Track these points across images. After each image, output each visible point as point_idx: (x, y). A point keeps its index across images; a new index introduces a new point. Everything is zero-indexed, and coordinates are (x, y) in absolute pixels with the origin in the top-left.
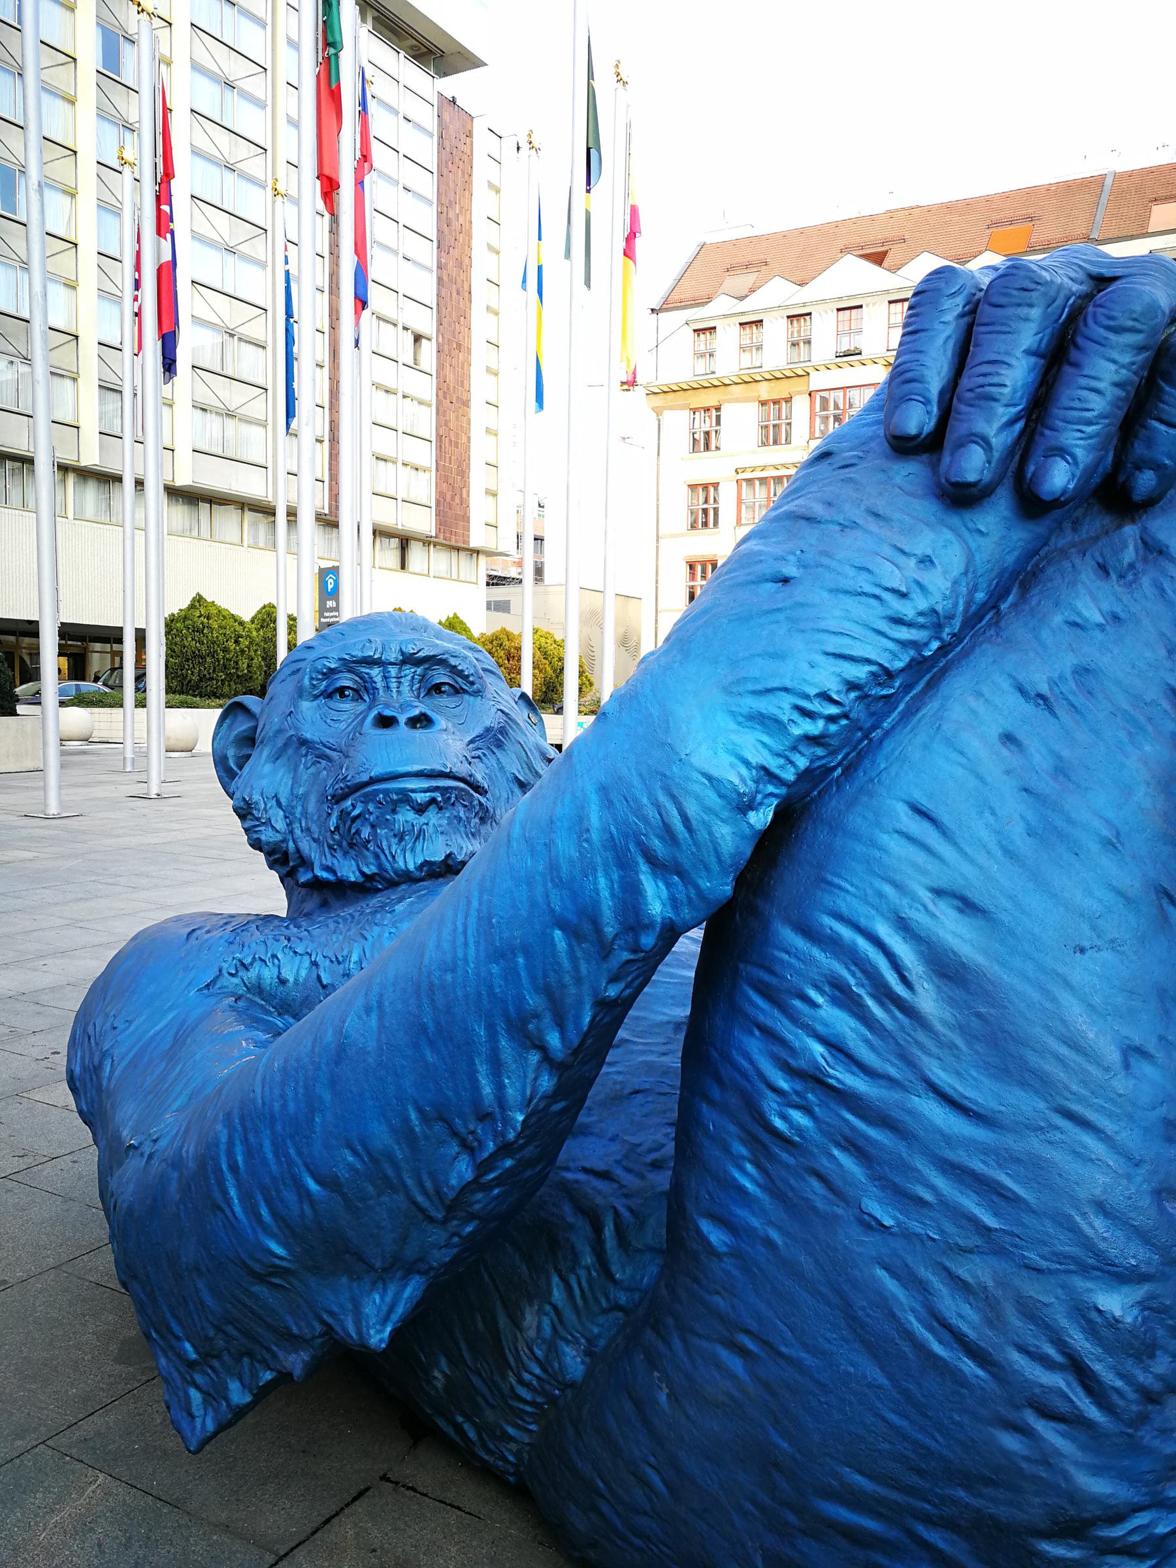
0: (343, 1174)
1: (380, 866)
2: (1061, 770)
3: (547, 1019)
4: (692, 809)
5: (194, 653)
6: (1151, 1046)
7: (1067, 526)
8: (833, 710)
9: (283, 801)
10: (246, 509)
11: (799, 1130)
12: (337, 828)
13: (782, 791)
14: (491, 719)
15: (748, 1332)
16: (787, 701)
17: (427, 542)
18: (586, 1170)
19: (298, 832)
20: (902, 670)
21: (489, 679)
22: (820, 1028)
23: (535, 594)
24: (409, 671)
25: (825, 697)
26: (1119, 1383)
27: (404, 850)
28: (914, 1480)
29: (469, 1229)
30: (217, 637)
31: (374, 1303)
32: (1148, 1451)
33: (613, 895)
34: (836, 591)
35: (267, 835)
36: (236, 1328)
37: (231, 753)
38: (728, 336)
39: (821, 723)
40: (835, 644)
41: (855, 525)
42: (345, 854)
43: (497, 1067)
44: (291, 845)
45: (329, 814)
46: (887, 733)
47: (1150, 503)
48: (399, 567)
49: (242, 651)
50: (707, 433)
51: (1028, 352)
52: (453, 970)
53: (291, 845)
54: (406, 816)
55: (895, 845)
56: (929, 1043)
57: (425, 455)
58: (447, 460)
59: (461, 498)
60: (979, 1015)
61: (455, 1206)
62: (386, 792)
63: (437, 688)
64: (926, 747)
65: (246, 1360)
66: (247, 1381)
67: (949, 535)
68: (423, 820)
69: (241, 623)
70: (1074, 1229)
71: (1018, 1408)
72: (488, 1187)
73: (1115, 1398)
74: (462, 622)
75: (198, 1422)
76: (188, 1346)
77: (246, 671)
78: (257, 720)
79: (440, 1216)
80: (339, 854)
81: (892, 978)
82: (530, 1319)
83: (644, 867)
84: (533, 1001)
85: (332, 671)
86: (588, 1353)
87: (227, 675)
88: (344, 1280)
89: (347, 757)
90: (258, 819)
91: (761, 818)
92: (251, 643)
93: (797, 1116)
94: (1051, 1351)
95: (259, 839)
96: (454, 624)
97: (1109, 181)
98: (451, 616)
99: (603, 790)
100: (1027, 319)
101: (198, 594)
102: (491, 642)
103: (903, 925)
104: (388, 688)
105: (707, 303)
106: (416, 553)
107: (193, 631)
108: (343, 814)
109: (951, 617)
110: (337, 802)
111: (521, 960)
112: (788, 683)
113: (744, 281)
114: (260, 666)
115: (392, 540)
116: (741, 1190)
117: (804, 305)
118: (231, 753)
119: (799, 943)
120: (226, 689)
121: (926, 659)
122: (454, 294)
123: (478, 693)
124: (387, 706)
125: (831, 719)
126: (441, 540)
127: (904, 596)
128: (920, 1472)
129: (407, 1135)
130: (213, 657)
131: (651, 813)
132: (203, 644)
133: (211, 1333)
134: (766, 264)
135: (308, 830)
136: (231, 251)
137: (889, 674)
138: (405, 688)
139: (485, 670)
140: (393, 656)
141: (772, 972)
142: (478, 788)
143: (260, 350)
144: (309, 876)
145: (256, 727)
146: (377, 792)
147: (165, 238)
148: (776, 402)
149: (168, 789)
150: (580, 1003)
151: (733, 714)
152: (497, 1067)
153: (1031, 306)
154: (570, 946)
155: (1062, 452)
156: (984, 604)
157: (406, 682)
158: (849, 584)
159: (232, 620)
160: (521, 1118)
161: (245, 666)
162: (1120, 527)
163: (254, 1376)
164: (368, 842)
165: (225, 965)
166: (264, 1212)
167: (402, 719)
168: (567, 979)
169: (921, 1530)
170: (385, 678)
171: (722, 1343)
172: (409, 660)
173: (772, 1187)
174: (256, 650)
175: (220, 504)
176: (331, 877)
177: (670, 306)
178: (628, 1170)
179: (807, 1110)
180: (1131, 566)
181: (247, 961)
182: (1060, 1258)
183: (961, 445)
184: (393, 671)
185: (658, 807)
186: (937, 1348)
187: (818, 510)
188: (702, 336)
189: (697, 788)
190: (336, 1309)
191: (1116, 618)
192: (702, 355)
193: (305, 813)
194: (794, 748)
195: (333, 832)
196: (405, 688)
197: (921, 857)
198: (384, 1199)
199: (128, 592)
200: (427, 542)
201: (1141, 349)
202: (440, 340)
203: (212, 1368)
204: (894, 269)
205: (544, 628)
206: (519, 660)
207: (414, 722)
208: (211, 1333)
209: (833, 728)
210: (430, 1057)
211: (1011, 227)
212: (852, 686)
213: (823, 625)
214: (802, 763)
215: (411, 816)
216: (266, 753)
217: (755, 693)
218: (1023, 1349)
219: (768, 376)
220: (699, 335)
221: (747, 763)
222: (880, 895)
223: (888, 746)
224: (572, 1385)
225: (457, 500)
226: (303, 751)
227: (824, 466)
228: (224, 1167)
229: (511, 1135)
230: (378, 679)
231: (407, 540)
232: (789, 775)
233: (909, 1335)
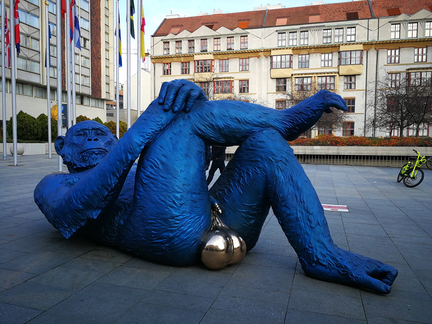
0: (90, 195)
1: (90, 164)
2: (176, 142)
3: (117, 172)
4: (134, 146)
5: (20, 127)
6: (183, 170)
7: (180, 114)
8: (151, 135)
9: (71, 154)
10: (34, 86)
11: (147, 182)
12: (81, 158)
13: (145, 144)
14: (109, 140)
15: (141, 206)
16: (145, 134)
17: (89, 97)
18: (124, 199)
19: (73, 159)
20: (159, 130)
21: (108, 132)
22: (149, 171)
23: (120, 111)
24: (93, 131)
25: (149, 133)
26: (178, 203)
27: (94, 161)
28: (157, 216)
29: (107, 203)
30: (27, 123)
31: (94, 213)
32: (181, 210)
33: (125, 157)
34: (151, 121)
35: (68, 160)
36: (74, 220)
37: (58, 146)
38: (172, 45)
39: (149, 136)
40: (151, 127)
41: (154, 113)
42: (83, 162)
43: (111, 179)
44: (72, 162)
45: (80, 156)
46: (158, 138)
47: (189, 112)
48: (81, 104)
49: (35, 127)
50: (167, 70)
51: (173, 94)
52: (105, 167)
53: (72, 162)
54: (94, 156)
55: (157, 150)
56: (160, 171)
57: (88, 73)
58: (95, 74)
59: (99, 85)
60: (166, 168)
61: (105, 198)
62: (90, 152)
63: (99, 134)
64: (162, 139)
65: (75, 226)
66: (75, 228)
67: (164, 115)
68: (97, 156)
69: (35, 119)
70: (174, 188)
71: (167, 206)
72: (110, 196)
73: (177, 205)
74: (100, 119)
75: (68, 235)
76: (66, 225)
77: (36, 133)
78: (64, 140)
79: (103, 200)
80: (82, 163)
81: (157, 165)
82: (116, 218)
83: (128, 153)
84: (115, 170)
85: (79, 131)
86: (124, 221)
87: (30, 134)
88: (90, 211)
89: (83, 146)
90: (66, 157)
91: (142, 147)
92: (38, 125)
93: (146, 181)
94: (171, 200)
95: (66, 161)
96: (97, 119)
97: (267, 12)
98: (96, 117)
99: (123, 144)
100: (173, 90)
101: (21, 111)
102: (108, 125)
103: (158, 159)
104: (90, 134)
105: (167, 35)
106: (86, 101)
107: (20, 121)
108: (83, 156)
109: (164, 124)
110: (81, 154)
111: (113, 165)
112: (145, 132)
113: (177, 30)
114: (41, 131)
115: (78, 96)
116: (141, 191)
117: (192, 37)
118: (58, 146)
119: (147, 161)
120: (30, 138)
121: (162, 129)
122: (96, 28)
123: (106, 135)
124: (90, 137)
125: (150, 136)
126: (93, 96)
127: (159, 122)
128: (158, 215)
129: (99, 189)
130: (26, 129)
131: (129, 147)
132: (23, 125)
133: (70, 221)
134: (182, 26)
135: (76, 159)
136: (28, 12)
137: (157, 131)
138: (93, 134)
139: (107, 131)
140: (90, 128)
141: (144, 165)
142: (107, 151)
143: (38, 41)
144: (76, 167)
145: (64, 142)
146: (89, 152)
147: (17, 19)
148: (186, 63)
149: (19, 164)
150: (121, 170)
151: (139, 135)
152: (111, 179)
153: (173, 89)
154: (120, 163)
155: (176, 106)
156: (169, 123)
157: (93, 133)
158: (152, 120)
159: (32, 118)
160: (114, 185)
161: (36, 131)
162: (186, 114)
163: (76, 227)
164: (87, 160)
165: (63, 180)
166: (79, 202)
167: (93, 139)
168: (119, 168)
169: (158, 221)
170: (89, 132)
171: (139, 209)
172: (93, 129)
173: (144, 190)
174: (39, 127)
175: (26, 85)
176: (80, 167)
177: (157, 35)
178: (130, 198)
179: (148, 180)
180: (186, 119)
181: (67, 179)
182: (172, 191)
183: (165, 105)
184: (90, 131)
185: (130, 146)
186: (160, 202)
187: (150, 111)
188: (166, 44)
189: (135, 144)
190: (89, 214)
191: (184, 125)
192: (166, 49)
193: (75, 156)
194: (146, 139)
195: (80, 159)
196: (93, 134)
197: (160, 151)
198: (96, 198)
199: (4, 111)
200: (89, 97)
201: (185, 94)
202: (92, 41)
203: (70, 228)
204: (215, 30)
205: (123, 121)
206: (116, 130)
207: (95, 140)
208: (70, 221)
209: (151, 137)
210: (102, 178)
211: (244, 22)
212: (153, 132)
213: (149, 125)
214: (147, 141)
215: (95, 155)
216: (67, 146)
217: (142, 133)
218: (168, 201)
219: (183, 56)
220: (165, 44)
221: (140, 141)
222: (156, 156)
223: (158, 139)
224: (122, 225)
225: (98, 86)
226: (74, 145)
227: (151, 105)
228: (72, 197)
229: (113, 187)
230: (88, 132)
231: (83, 96)
232: (146, 142)
233: (157, 201)
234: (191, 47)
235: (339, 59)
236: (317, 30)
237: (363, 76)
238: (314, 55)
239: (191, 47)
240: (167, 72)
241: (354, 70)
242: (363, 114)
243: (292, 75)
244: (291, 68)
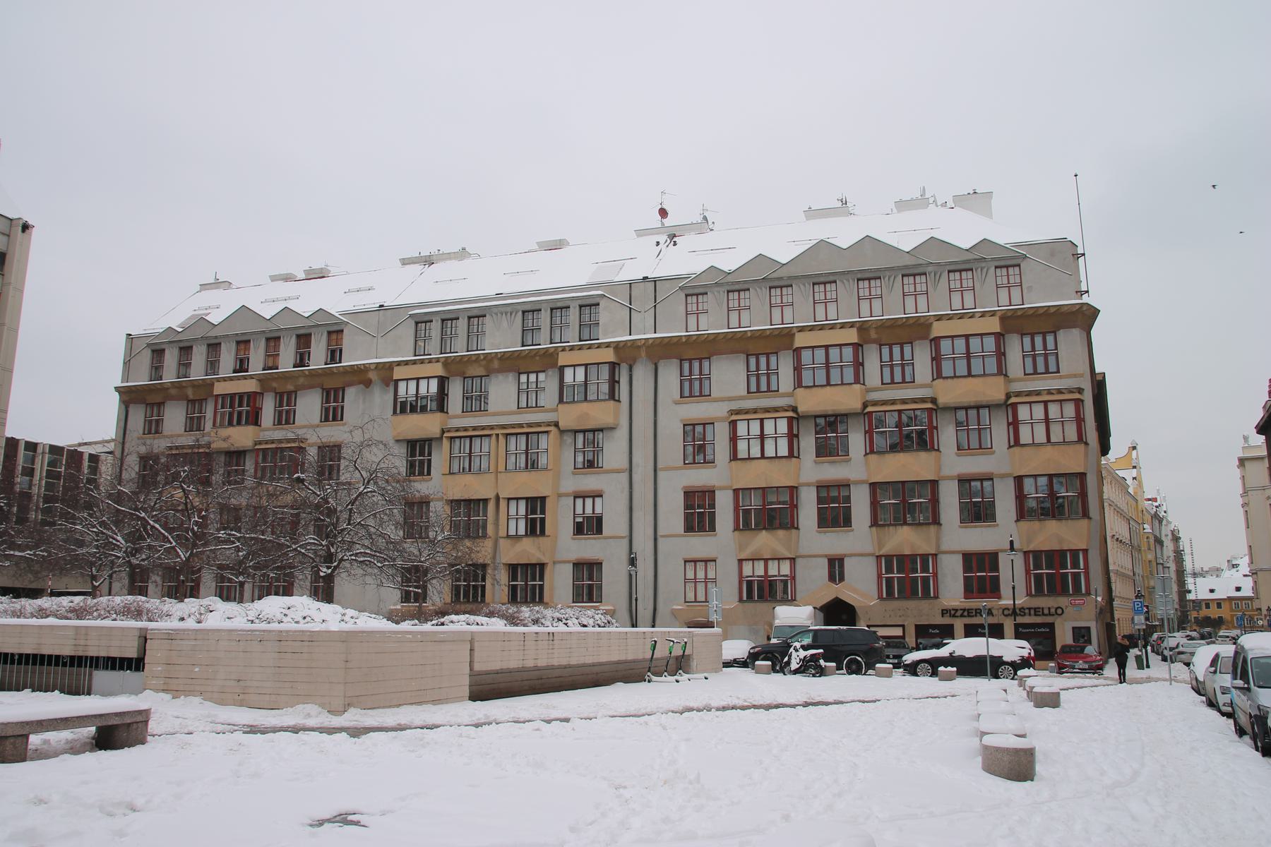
117: (216, 337)
234: (213, 365)
235: (933, 359)
236: (506, 314)
237: (622, 432)
238: (501, 377)
239: (213, 365)
240: (154, 427)
241: (599, 413)
242: (663, 536)
243: (443, 432)
244: (859, 383)
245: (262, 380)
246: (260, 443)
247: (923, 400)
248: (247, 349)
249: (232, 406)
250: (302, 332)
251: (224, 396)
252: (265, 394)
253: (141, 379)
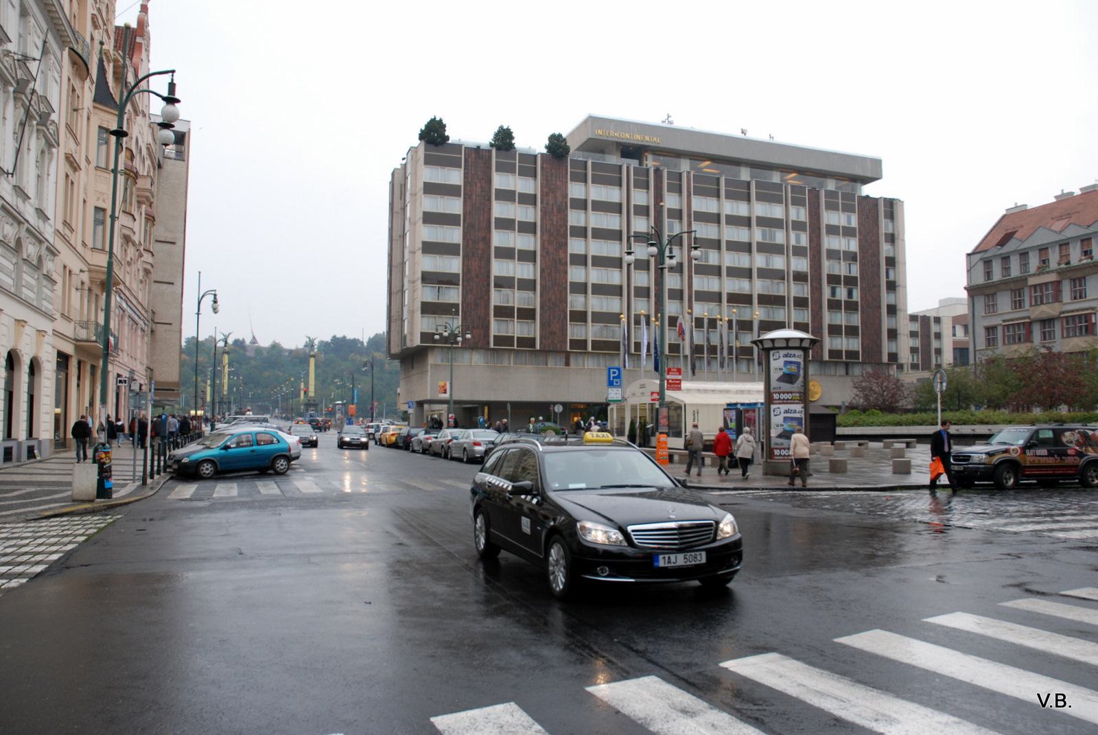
117: (1025, 249)
239: (1024, 265)
245: (1060, 272)
246: (1064, 313)
247: (1024, 318)
248: (1047, 254)
249: (1041, 291)
250: (33, 460)
251: (1035, 286)
252: (1087, 278)
253: (980, 280)
